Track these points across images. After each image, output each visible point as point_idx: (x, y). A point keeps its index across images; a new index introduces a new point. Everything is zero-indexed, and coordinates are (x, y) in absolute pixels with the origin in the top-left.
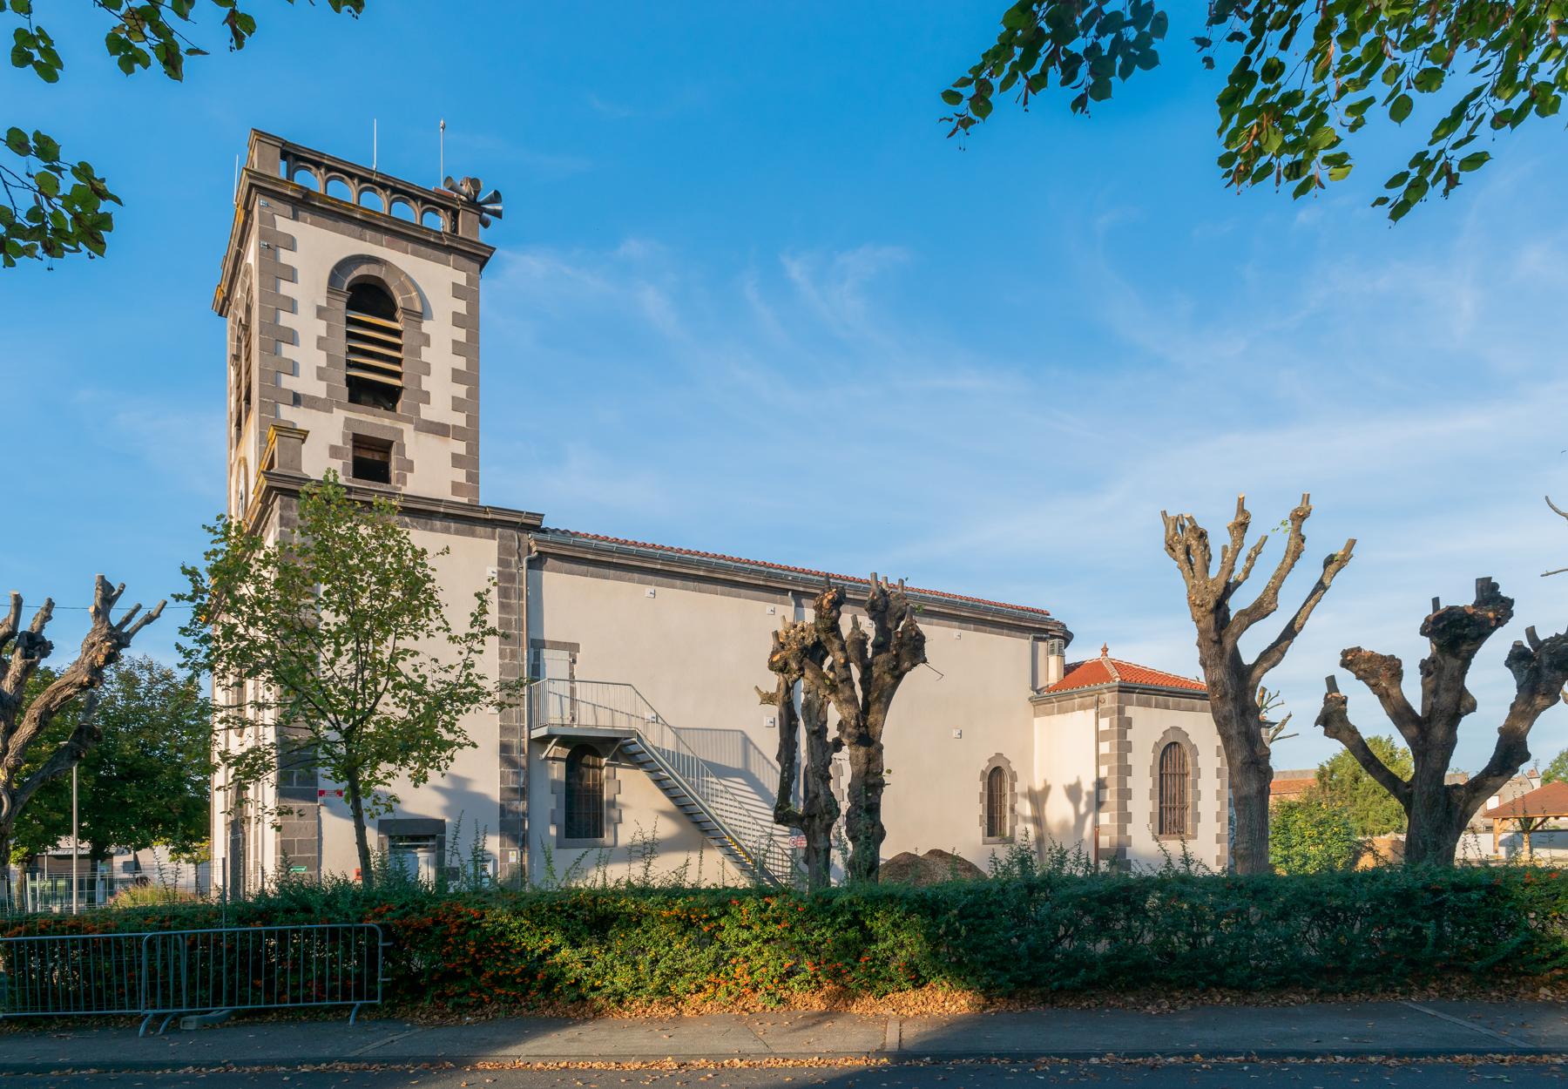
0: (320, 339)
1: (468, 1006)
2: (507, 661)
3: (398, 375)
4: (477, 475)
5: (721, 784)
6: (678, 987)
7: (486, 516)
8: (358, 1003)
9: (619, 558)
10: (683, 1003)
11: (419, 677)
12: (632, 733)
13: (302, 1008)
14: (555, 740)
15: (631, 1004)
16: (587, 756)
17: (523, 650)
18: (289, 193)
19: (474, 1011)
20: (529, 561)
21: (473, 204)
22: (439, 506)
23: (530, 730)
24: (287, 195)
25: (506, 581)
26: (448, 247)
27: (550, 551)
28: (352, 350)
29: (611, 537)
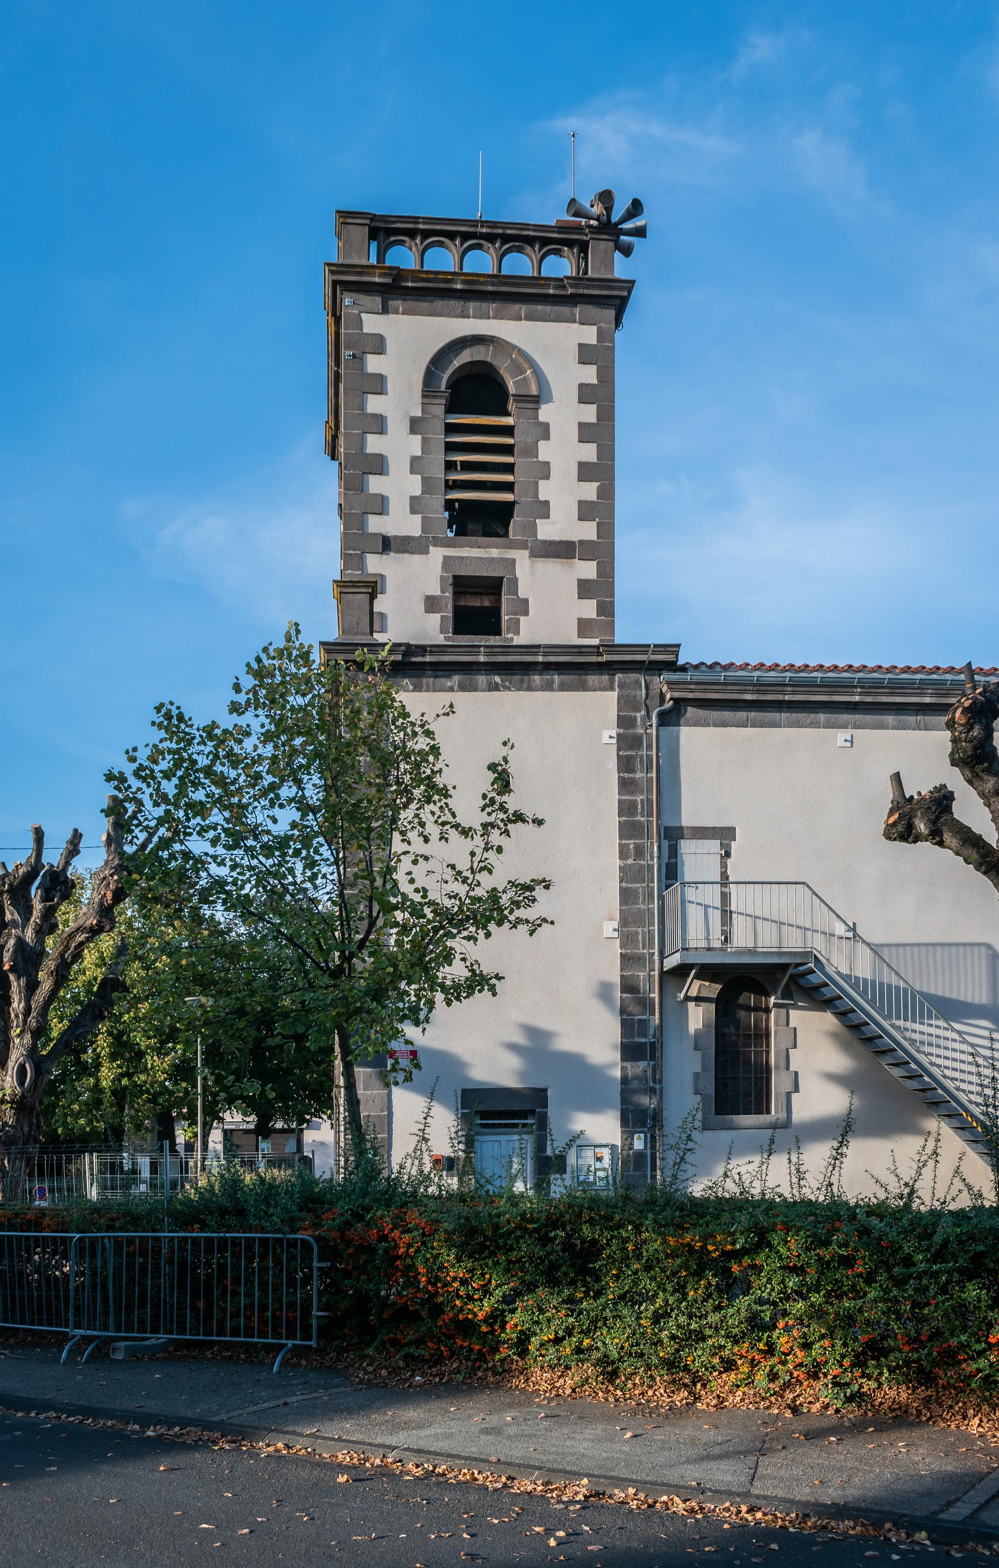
0: (414, 460)
1: (424, 1361)
2: (630, 861)
3: (509, 487)
4: (612, 604)
5: (953, 1030)
6: (698, 1357)
7: (600, 659)
8: (290, 1343)
9: (793, 693)
10: (704, 1386)
11: (417, 891)
12: (806, 954)
13: (242, 1344)
14: (694, 972)
15: (627, 1379)
16: (745, 994)
17: (652, 844)
18: (377, 280)
19: (430, 1368)
20: (661, 715)
21: (608, 229)
22: (536, 654)
23: (662, 957)
24: (375, 283)
25: (631, 747)
26: (573, 296)
27: (691, 696)
28: (450, 466)
29: (783, 664)
